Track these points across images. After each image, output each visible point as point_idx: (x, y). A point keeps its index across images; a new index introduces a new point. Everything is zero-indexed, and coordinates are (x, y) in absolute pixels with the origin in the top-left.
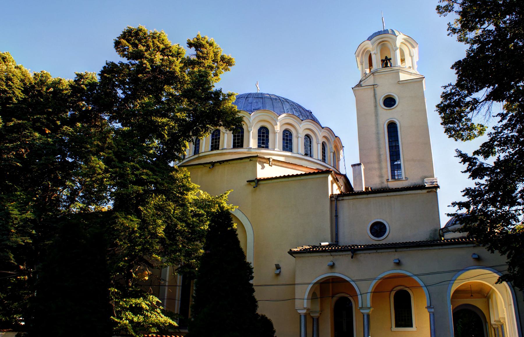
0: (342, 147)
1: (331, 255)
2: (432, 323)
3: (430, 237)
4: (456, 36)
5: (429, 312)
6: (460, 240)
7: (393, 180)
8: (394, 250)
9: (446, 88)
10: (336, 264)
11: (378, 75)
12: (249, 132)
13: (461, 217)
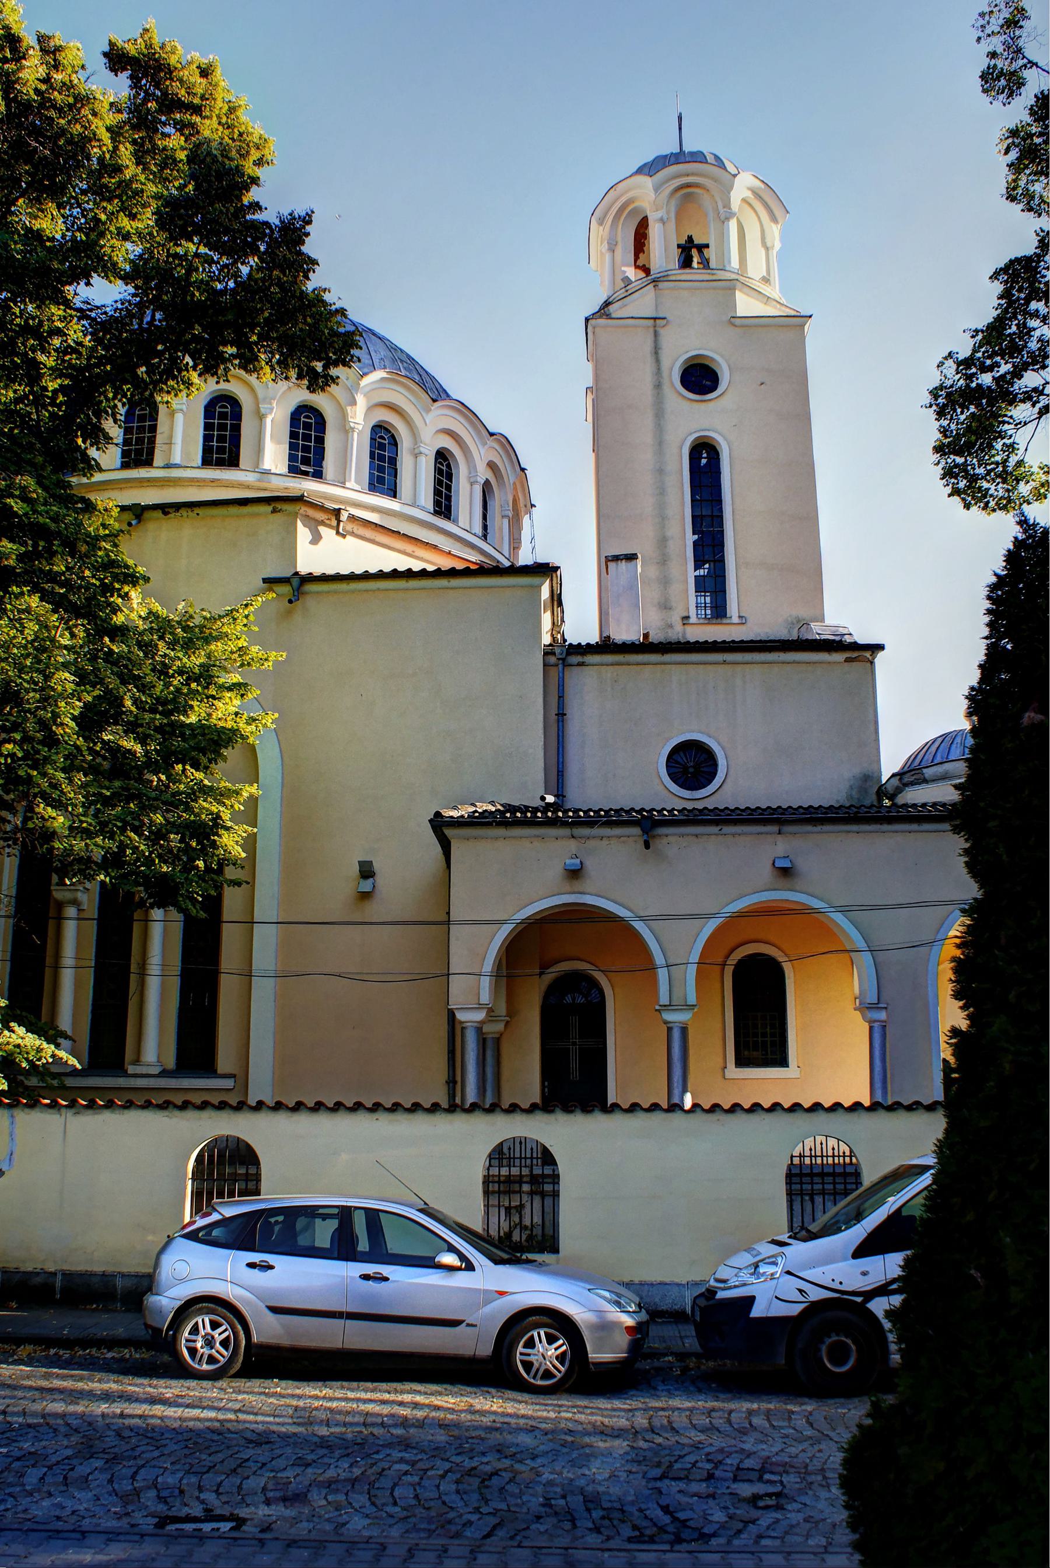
1: (573, 837)
3: (850, 797)
5: (871, 1022)
8: (775, 828)
10: (589, 864)
12: (261, 417)
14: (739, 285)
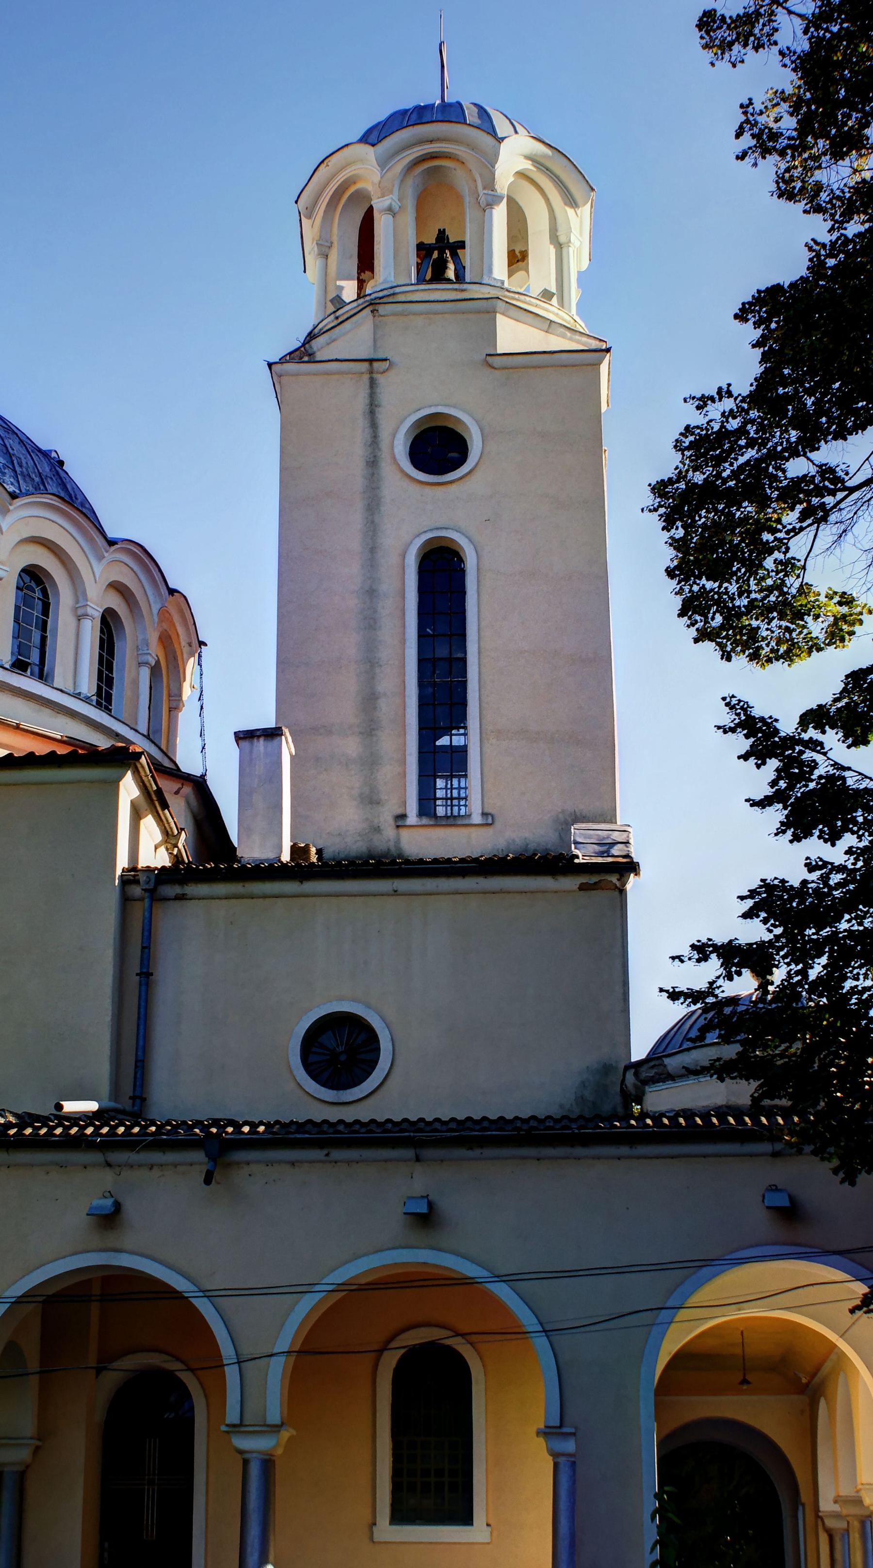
0: (195, 643)
1: (109, 1165)
2: (563, 1505)
3: (581, 1100)
4: (771, 166)
5: (555, 1455)
6: (715, 1120)
7: (425, 821)
8: (410, 1153)
9: (706, 405)
10: (130, 1207)
11: (395, 314)
13: (727, 1010)
14: (500, 304)
